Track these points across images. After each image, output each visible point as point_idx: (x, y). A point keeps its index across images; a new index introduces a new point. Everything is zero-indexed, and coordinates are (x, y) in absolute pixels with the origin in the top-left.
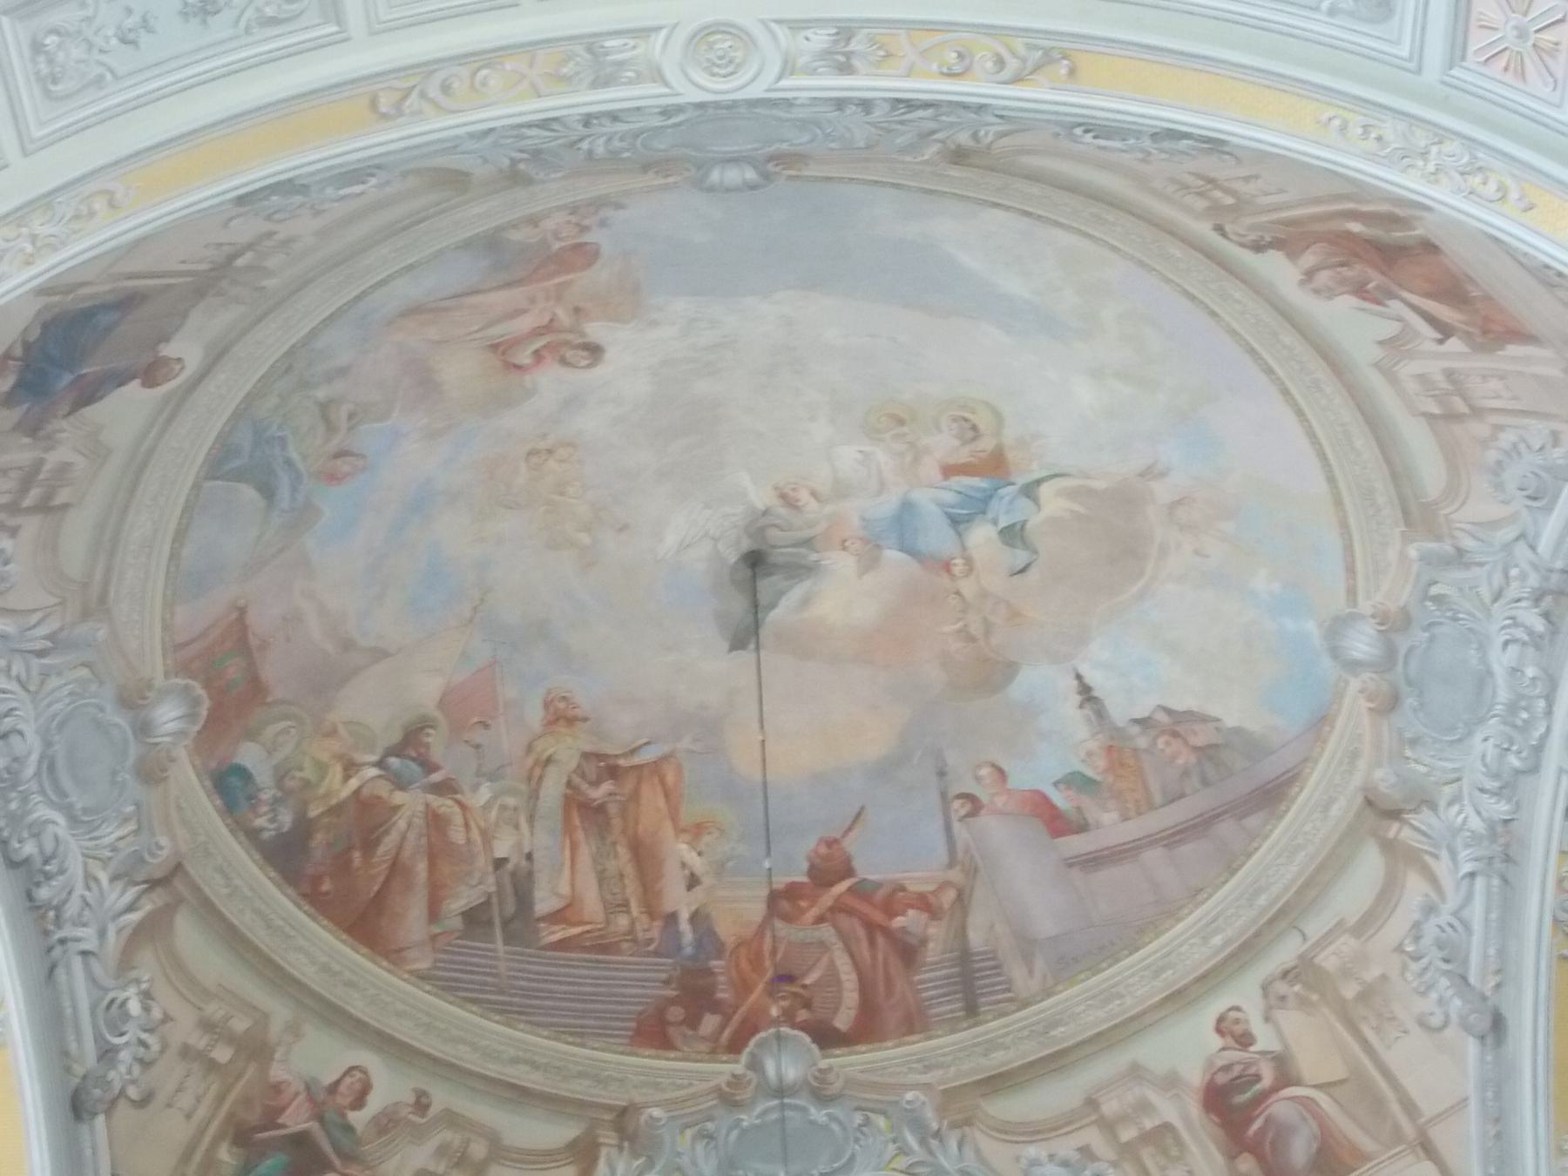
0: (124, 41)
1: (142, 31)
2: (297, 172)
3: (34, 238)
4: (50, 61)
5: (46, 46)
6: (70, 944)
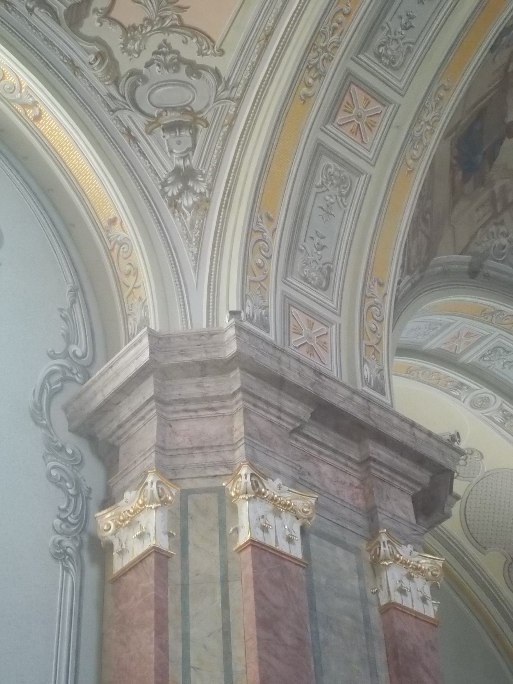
0: (406, 29)
1: (411, 21)
2: (506, 22)
3: (428, 123)
4: (387, 57)
5: (381, 53)
6: (161, 495)
